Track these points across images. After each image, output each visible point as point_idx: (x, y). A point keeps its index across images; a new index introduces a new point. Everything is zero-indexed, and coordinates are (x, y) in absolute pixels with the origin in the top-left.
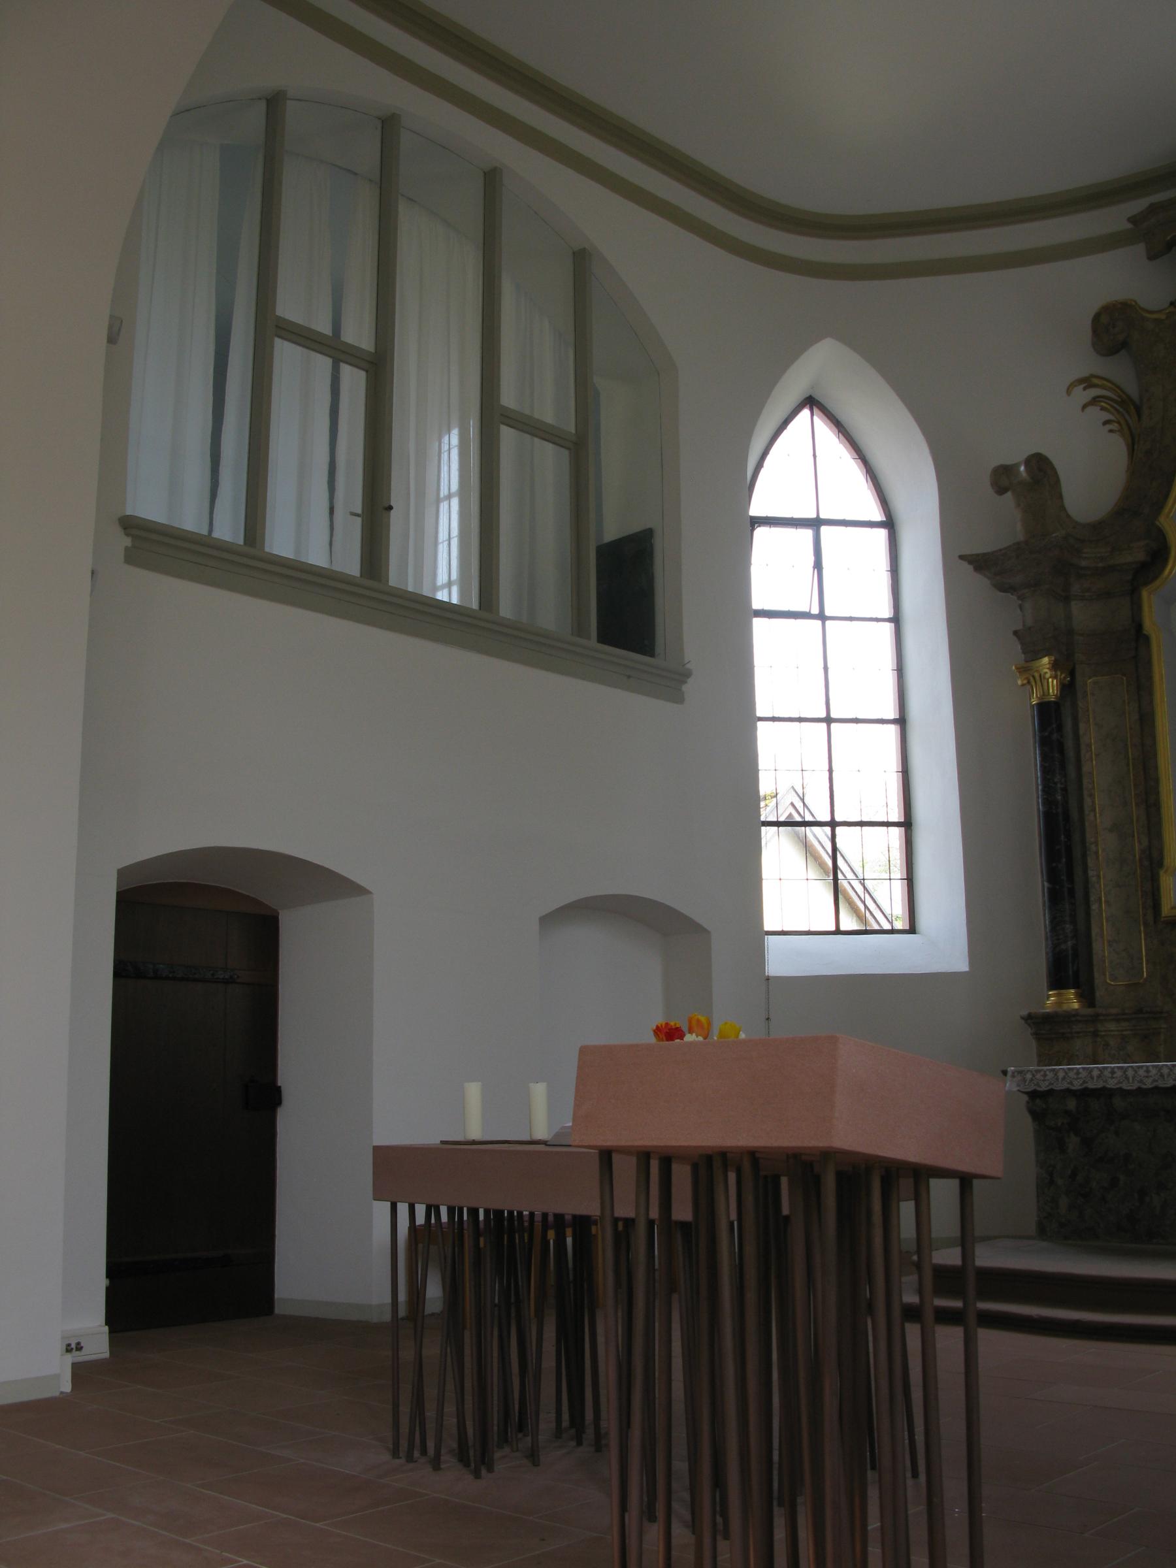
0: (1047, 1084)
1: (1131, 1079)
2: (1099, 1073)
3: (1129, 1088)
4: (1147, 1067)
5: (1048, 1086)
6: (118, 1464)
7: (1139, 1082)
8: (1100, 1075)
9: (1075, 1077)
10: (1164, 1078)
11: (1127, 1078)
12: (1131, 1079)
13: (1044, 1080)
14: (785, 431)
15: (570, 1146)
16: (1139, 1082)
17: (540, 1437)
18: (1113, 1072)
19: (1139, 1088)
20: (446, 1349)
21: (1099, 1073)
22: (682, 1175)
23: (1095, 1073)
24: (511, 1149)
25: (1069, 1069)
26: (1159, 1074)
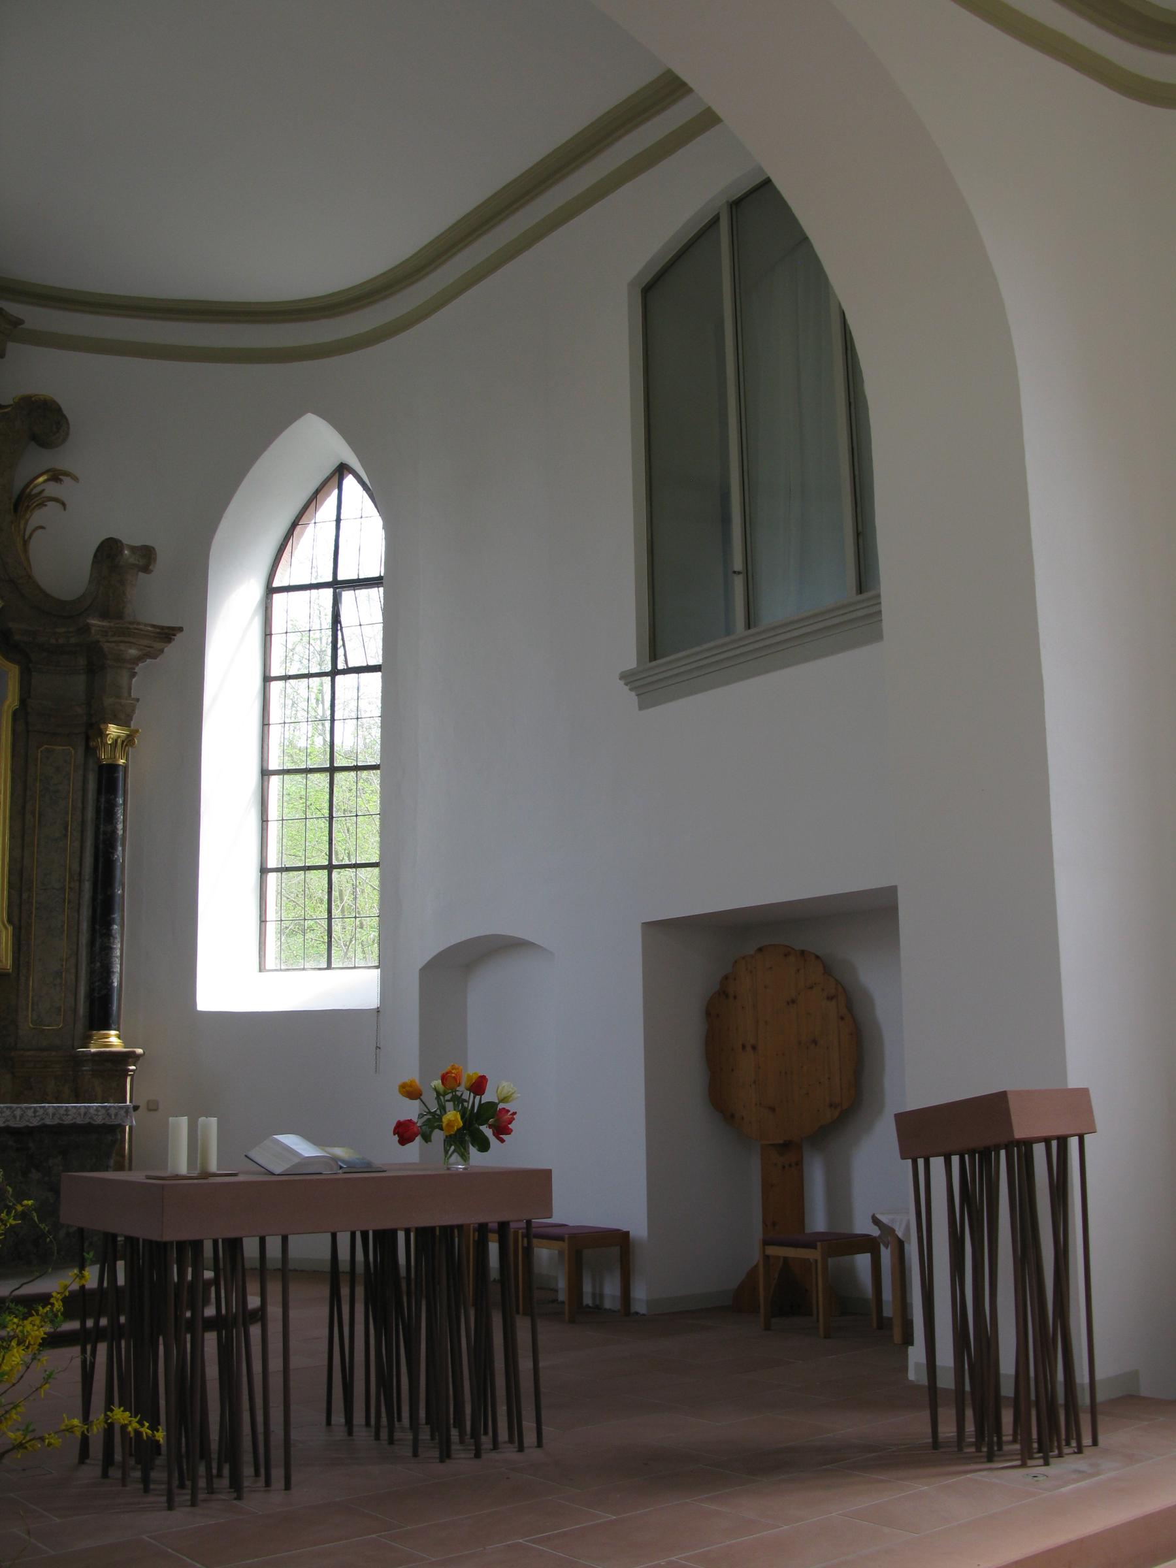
0: (39, 1119)
1: (18, 1118)
2: (55, 1111)
3: (15, 1126)
4: (35, 1108)
5: (39, 1121)
6: (567, 1503)
7: (90, 1118)
8: (22, 1114)
9: (96, 1113)
10: (111, 1118)
11: (14, 1117)
12: (18, 1118)
13: (35, 1117)
14: (332, 571)
15: (321, 1173)
16: (90, 1118)
17: (411, 1437)
18: (35, 1111)
19: (90, 1123)
20: (179, 1440)
21: (55, 1111)
22: (1054, 1143)
23: (18, 1113)
24: (281, 1179)
25: (58, 1107)
26: (12, 1115)
